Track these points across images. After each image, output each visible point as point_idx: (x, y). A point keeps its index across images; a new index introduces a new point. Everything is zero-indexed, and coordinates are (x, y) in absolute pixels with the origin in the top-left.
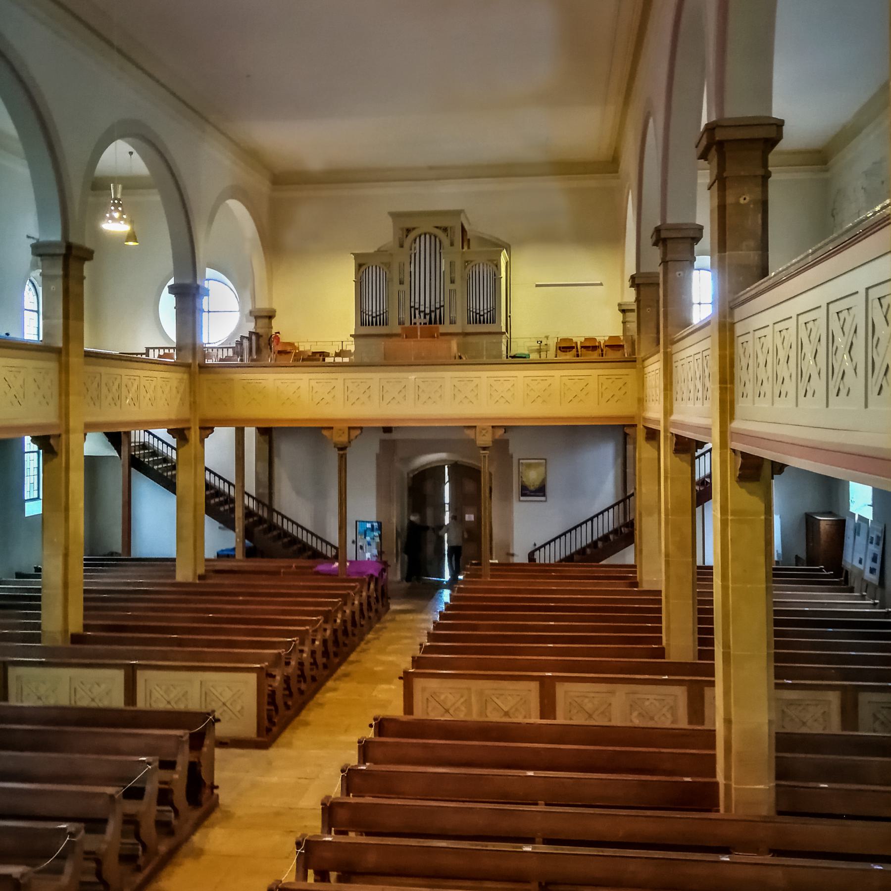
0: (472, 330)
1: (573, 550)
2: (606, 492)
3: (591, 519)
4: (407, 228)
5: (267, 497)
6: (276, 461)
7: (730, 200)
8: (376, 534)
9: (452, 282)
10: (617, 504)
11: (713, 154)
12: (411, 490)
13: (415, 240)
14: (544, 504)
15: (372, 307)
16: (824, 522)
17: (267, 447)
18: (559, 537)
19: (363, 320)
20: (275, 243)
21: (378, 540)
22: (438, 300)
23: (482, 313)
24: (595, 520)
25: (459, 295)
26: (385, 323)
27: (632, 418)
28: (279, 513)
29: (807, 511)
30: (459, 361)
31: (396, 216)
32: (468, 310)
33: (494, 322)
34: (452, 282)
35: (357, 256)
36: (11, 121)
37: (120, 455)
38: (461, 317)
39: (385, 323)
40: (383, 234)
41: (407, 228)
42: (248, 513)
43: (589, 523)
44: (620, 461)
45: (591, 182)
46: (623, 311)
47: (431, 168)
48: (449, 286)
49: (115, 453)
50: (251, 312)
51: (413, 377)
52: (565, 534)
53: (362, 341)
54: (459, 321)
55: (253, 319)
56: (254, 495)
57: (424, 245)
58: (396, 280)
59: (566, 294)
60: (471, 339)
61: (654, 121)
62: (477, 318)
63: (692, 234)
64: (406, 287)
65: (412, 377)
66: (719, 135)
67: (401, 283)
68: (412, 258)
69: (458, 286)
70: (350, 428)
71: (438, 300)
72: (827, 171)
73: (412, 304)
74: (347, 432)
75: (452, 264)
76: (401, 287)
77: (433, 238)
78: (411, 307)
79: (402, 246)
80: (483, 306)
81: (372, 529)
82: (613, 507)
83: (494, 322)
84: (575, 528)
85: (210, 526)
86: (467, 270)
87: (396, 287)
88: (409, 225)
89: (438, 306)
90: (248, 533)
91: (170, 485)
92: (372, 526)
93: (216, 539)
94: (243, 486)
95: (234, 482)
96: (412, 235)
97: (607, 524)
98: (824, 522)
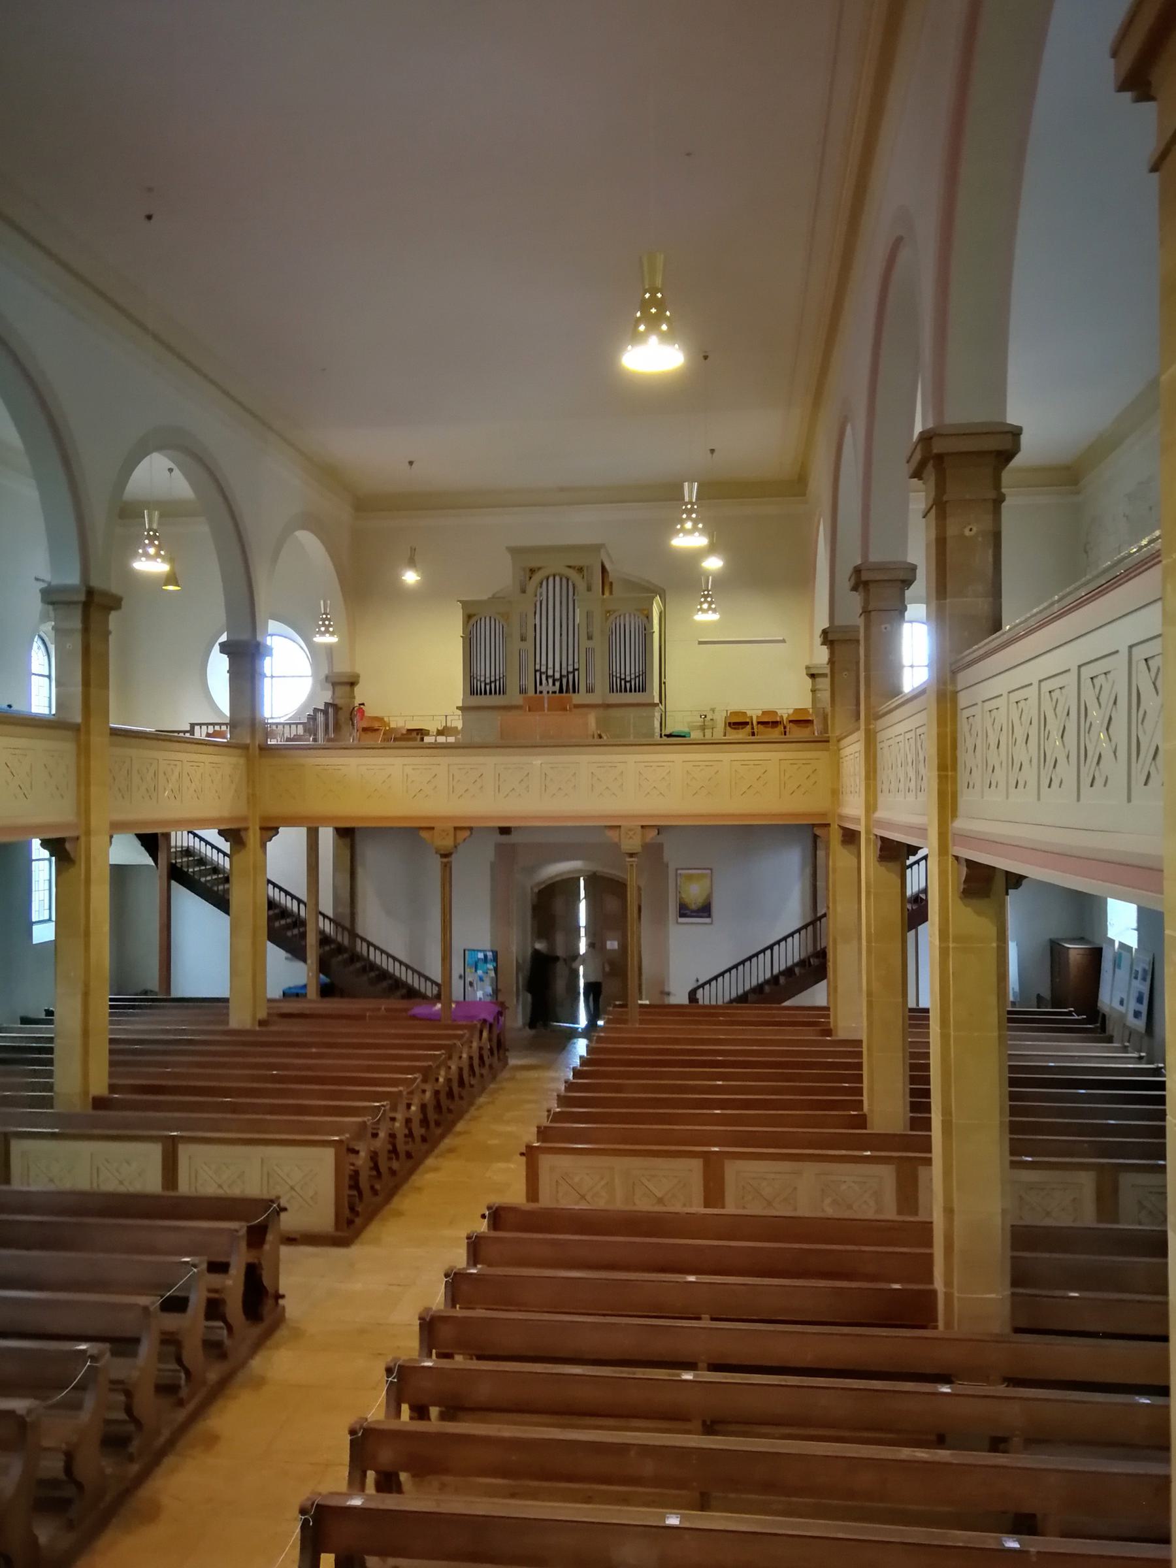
1: (747, 988)
3: (771, 947)
4: (531, 568)
5: (347, 920)
6: (360, 871)
7: (952, 530)
8: (490, 966)
9: (590, 638)
10: (805, 927)
13: (541, 583)
15: (484, 671)
16: (1075, 950)
19: (473, 687)
21: (492, 974)
22: (570, 662)
23: (628, 679)
24: (776, 948)
27: (824, 815)
28: (363, 939)
29: (1052, 936)
32: (611, 675)
33: (644, 690)
35: (465, 604)
37: (156, 863)
38: (601, 683)
39: (501, 691)
40: (500, 576)
42: (324, 940)
43: (768, 952)
44: (808, 871)
46: (813, 676)
48: (585, 643)
49: (150, 862)
52: (736, 966)
58: (517, 636)
62: (622, 685)
63: (902, 575)
65: (537, 762)
66: (938, 447)
67: (523, 639)
71: (570, 662)
72: (1078, 493)
73: (538, 667)
75: (589, 615)
76: (523, 645)
77: (564, 581)
79: (524, 591)
80: (630, 670)
82: (798, 931)
83: (644, 690)
85: (275, 955)
88: (534, 565)
89: (571, 669)
90: (324, 966)
91: (222, 903)
92: (486, 956)
93: (284, 972)
95: (305, 899)
96: (537, 577)
97: (790, 954)
98: (1075, 950)
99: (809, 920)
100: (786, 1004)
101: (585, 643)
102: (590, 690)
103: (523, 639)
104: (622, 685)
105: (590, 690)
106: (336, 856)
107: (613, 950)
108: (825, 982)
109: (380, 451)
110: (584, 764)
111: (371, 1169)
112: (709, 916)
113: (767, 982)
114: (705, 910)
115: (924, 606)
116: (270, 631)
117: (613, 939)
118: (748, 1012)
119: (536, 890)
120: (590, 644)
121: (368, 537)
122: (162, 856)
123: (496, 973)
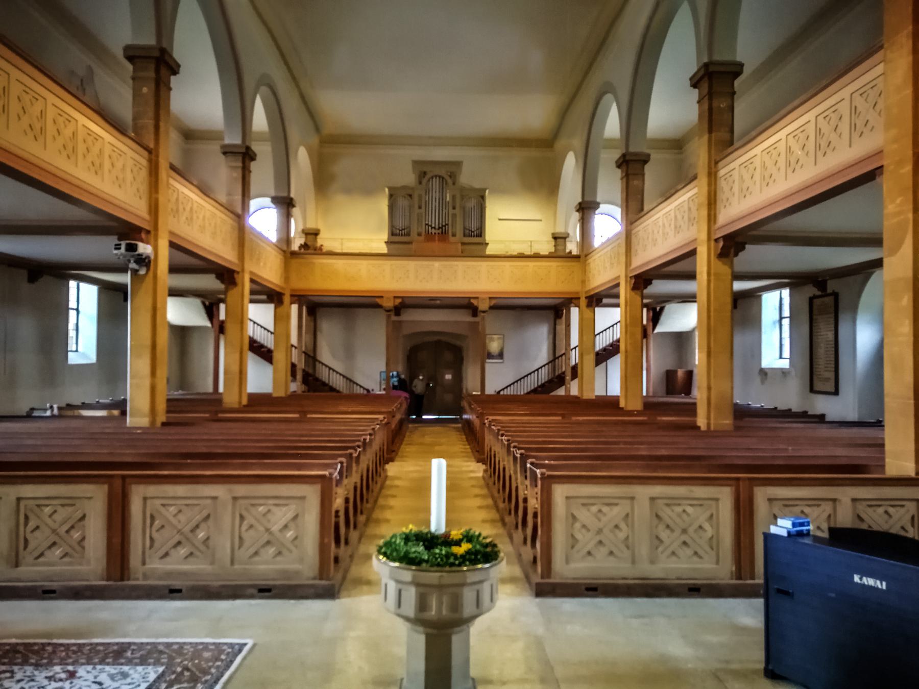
0: (471, 240)
2: (542, 355)
3: (537, 370)
4: (423, 171)
5: (311, 357)
6: (318, 334)
7: (715, 104)
11: (705, 86)
15: (400, 224)
16: (680, 373)
17: (312, 324)
18: (513, 383)
20: (323, 182)
25: (458, 219)
26: (408, 234)
27: (577, 293)
29: (668, 368)
30: (463, 255)
31: (416, 163)
32: (465, 228)
33: (481, 236)
36: (910, 8)
38: (459, 233)
39: (408, 234)
40: (408, 178)
41: (423, 171)
44: (551, 336)
45: (534, 153)
47: (430, 137)
48: (451, 211)
49: (209, 324)
50: (303, 231)
52: (517, 381)
53: (393, 246)
54: (458, 235)
55: (304, 236)
57: (436, 183)
58: (416, 206)
59: (515, 225)
60: (466, 247)
61: (295, 220)
64: (423, 210)
65: (437, 264)
67: (420, 207)
68: (427, 192)
69: (458, 211)
70: (395, 297)
72: (681, 153)
75: (454, 197)
79: (420, 183)
80: (474, 226)
83: (481, 236)
84: (520, 379)
87: (417, 210)
97: (544, 375)
98: (680, 373)
100: (552, 394)
101: (451, 211)
102: (454, 235)
104: (468, 233)
105: (454, 235)
108: (597, 349)
109: (347, 107)
110: (461, 266)
111: (570, 252)
113: (539, 387)
114: (501, 355)
117: (443, 377)
118: (532, 396)
120: (454, 211)
121: (336, 157)
122: (215, 320)
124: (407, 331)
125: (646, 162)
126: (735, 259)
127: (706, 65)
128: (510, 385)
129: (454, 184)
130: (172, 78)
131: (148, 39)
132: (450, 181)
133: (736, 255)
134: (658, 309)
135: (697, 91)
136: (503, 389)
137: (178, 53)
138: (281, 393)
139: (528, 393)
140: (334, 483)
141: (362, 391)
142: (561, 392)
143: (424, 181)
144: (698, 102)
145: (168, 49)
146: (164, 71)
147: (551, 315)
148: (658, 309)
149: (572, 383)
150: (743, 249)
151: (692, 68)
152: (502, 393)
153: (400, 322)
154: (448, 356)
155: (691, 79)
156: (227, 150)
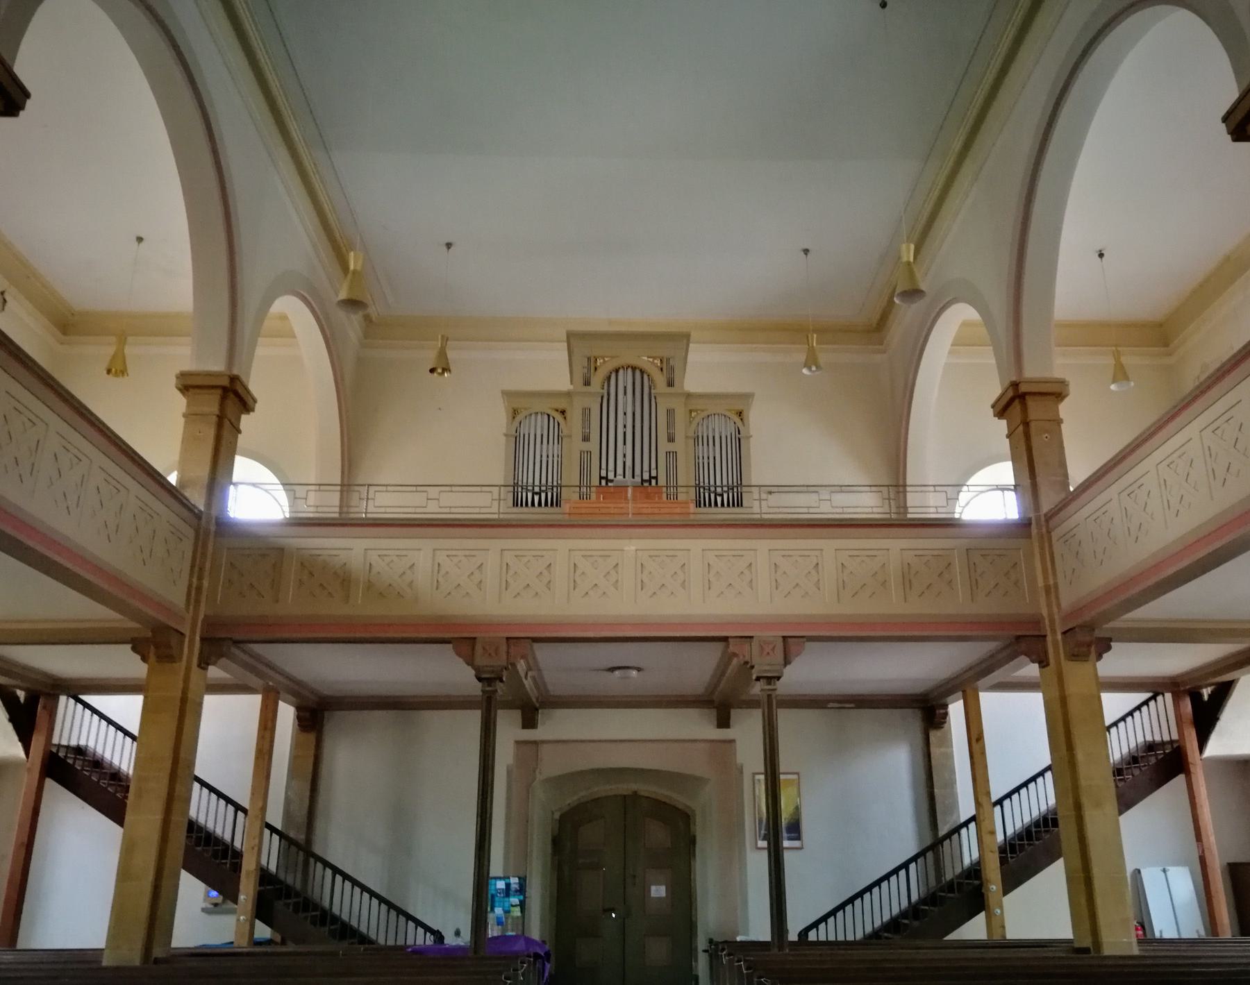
1: (878, 923)
2: (900, 837)
5: (300, 845)
8: (515, 900)
9: (671, 439)
10: (921, 854)
12: (556, 842)
13: (609, 378)
14: (800, 852)
21: (517, 912)
22: (646, 467)
23: (719, 490)
24: (1007, 803)
26: (557, 503)
28: (326, 864)
29: (1232, 860)
34: (671, 439)
37: (27, 754)
42: (265, 877)
43: (902, 873)
49: (18, 751)
51: (633, 548)
56: (279, 826)
58: (577, 436)
64: (593, 445)
67: (586, 439)
71: (646, 467)
73: (603, 474)
74: (504, 648)
76: (586, 446)
77: (638, 373)
78: (601, 478)
80: (722, 478)
81: (507, 891)
82: (914, 859)
85: (191, 891)
86: (694, 425)
88: (568, 414)
89: (646, 476)
90: (263, 911)
91: (116, 812)
92: (508, 885)
93: (200, 919)
94: (264, 809)
95: (245, 803)
99: (928, 842)
100: (953, 936)
101: (664, 446)
103: (586, 439)
106: (295, 759)
107: (660, 899)
112: (799, 838)
113: (903, 914)
115: (1009, 464)
116: (235, 478)
117: (658, 883)
119: (557, 816)
122: (38, 742)
123: (523, 911)
124: (552, 765)
125: (1059, 396)
126: (1099, 664)
127: (1015, 385)
128: (833, 913)
129: (670, 384)
130: (244, 418)
131: (216, 364)
132: (660, 380)
133: (1099, 657)
134: (1206, 693)
135: (1004, 423)
136: (815, 925)
137: (255, 385)
138: (243, 944)
139: (876, 935)
140: (553, 958)
141: (422, 939)
142: (975, 929)
143: (597, 380)
144: (1008, 436)
145: (243, 378)
146: (231, 403)
147: (913, 720)
148: (1206, 693)
149: (1008, 900)
150: (1109, 648)
151: (994, 389)
152: (812, 936)
153: (535, 743)
154: (657, 835)
155: (993, 407)
156: (190, 382)
